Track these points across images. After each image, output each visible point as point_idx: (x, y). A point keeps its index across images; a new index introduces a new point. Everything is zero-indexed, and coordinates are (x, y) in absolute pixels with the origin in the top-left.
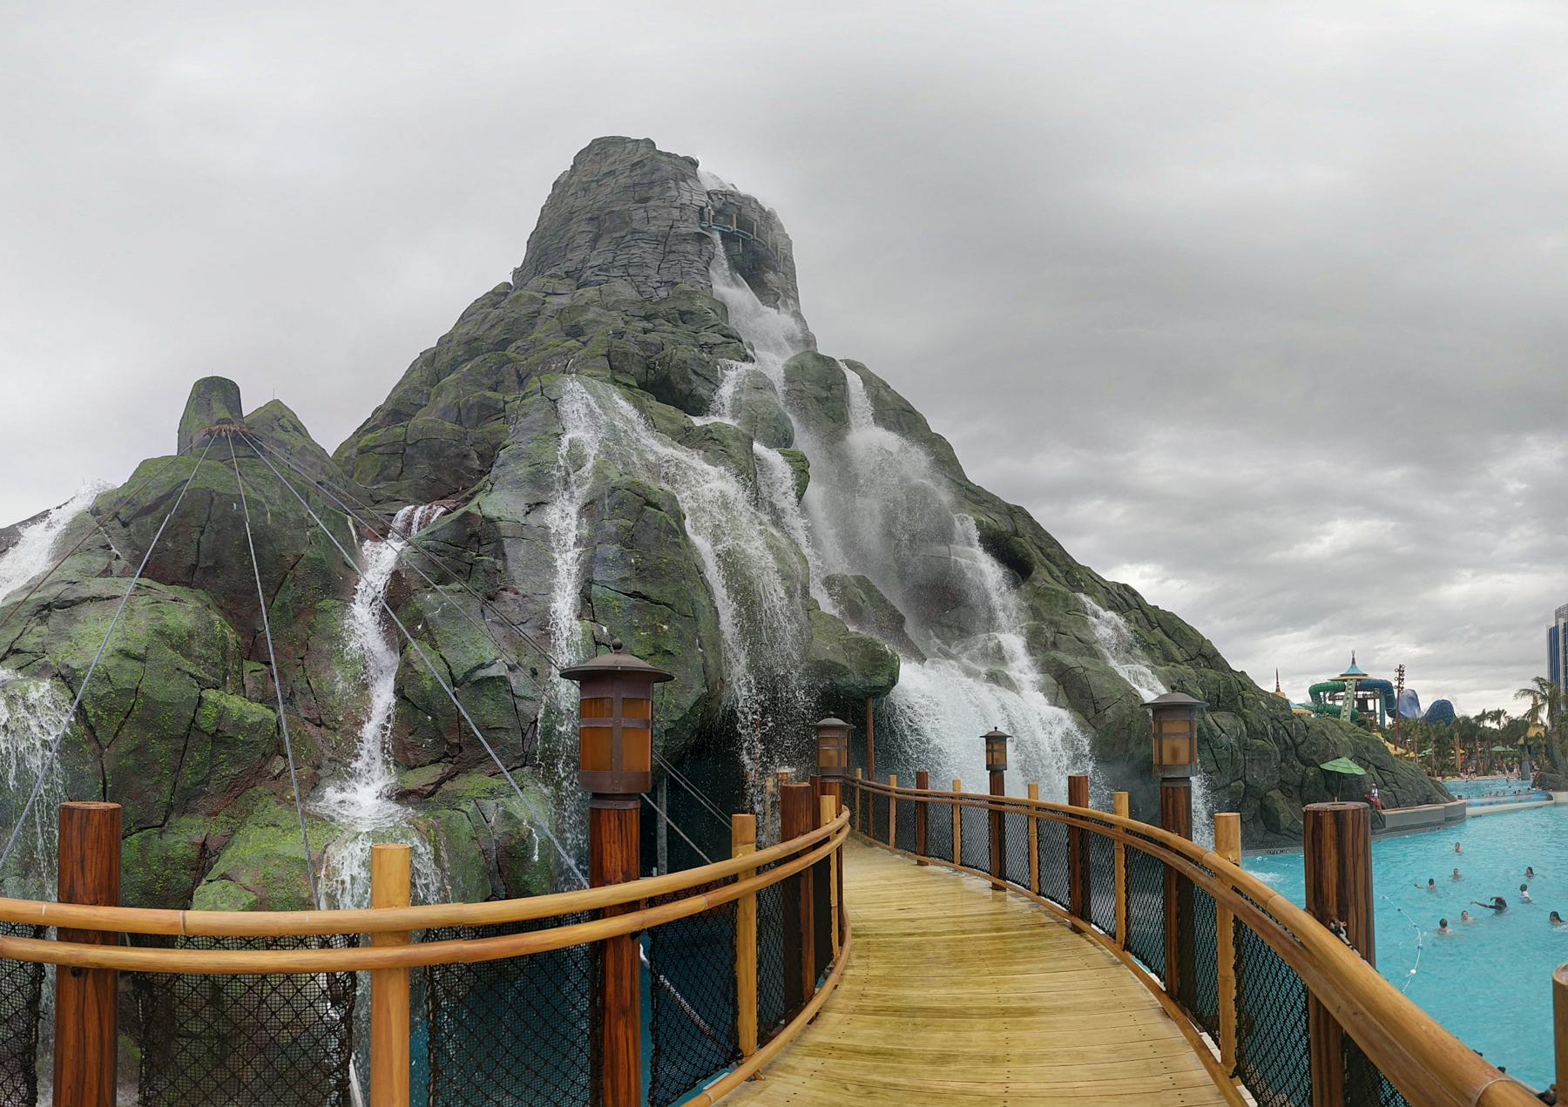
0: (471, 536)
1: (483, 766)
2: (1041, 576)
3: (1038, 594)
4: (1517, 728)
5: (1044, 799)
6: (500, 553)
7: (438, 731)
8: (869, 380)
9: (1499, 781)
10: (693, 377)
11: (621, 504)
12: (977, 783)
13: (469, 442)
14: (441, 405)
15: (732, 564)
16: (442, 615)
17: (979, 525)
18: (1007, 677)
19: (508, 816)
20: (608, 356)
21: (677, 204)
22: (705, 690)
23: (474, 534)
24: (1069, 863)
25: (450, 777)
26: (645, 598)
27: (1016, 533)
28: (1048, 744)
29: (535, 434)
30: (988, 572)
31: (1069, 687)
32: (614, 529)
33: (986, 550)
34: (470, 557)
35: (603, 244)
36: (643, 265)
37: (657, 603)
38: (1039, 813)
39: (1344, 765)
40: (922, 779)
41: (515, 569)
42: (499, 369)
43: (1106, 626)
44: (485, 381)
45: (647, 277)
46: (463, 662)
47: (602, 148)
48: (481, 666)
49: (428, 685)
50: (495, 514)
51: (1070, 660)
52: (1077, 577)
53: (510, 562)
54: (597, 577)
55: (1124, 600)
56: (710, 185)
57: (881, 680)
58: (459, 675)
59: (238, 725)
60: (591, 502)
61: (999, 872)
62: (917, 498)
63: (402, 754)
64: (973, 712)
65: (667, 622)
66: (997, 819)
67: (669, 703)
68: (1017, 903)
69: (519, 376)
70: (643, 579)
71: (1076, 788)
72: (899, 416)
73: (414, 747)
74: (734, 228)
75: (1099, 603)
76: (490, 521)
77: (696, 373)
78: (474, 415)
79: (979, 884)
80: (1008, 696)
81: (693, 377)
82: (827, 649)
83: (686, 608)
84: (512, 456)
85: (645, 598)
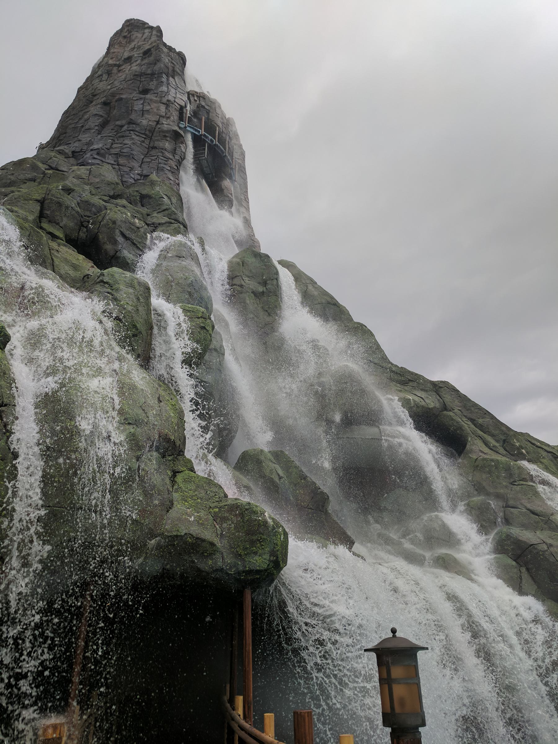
2: (477, 447)
3: (478, 466)
8: (300, 278)
10: (120, 239)
15: (57, 410)
17: (406, 403)
18: (455, 561)
21: (164, 100)
27: (445, 408)
30: (423, 449)
33: (418, 428)
35: (107, 131)
36: (130, 157)
45: (132, 169)
51: (528, 536)
56: (191, 87)
57: (259, 561)
62: (346, 380)
72: (328, 308)
74: (202, 132)
75: (547, 469)
80: (456, 584)
82: (187, 518)
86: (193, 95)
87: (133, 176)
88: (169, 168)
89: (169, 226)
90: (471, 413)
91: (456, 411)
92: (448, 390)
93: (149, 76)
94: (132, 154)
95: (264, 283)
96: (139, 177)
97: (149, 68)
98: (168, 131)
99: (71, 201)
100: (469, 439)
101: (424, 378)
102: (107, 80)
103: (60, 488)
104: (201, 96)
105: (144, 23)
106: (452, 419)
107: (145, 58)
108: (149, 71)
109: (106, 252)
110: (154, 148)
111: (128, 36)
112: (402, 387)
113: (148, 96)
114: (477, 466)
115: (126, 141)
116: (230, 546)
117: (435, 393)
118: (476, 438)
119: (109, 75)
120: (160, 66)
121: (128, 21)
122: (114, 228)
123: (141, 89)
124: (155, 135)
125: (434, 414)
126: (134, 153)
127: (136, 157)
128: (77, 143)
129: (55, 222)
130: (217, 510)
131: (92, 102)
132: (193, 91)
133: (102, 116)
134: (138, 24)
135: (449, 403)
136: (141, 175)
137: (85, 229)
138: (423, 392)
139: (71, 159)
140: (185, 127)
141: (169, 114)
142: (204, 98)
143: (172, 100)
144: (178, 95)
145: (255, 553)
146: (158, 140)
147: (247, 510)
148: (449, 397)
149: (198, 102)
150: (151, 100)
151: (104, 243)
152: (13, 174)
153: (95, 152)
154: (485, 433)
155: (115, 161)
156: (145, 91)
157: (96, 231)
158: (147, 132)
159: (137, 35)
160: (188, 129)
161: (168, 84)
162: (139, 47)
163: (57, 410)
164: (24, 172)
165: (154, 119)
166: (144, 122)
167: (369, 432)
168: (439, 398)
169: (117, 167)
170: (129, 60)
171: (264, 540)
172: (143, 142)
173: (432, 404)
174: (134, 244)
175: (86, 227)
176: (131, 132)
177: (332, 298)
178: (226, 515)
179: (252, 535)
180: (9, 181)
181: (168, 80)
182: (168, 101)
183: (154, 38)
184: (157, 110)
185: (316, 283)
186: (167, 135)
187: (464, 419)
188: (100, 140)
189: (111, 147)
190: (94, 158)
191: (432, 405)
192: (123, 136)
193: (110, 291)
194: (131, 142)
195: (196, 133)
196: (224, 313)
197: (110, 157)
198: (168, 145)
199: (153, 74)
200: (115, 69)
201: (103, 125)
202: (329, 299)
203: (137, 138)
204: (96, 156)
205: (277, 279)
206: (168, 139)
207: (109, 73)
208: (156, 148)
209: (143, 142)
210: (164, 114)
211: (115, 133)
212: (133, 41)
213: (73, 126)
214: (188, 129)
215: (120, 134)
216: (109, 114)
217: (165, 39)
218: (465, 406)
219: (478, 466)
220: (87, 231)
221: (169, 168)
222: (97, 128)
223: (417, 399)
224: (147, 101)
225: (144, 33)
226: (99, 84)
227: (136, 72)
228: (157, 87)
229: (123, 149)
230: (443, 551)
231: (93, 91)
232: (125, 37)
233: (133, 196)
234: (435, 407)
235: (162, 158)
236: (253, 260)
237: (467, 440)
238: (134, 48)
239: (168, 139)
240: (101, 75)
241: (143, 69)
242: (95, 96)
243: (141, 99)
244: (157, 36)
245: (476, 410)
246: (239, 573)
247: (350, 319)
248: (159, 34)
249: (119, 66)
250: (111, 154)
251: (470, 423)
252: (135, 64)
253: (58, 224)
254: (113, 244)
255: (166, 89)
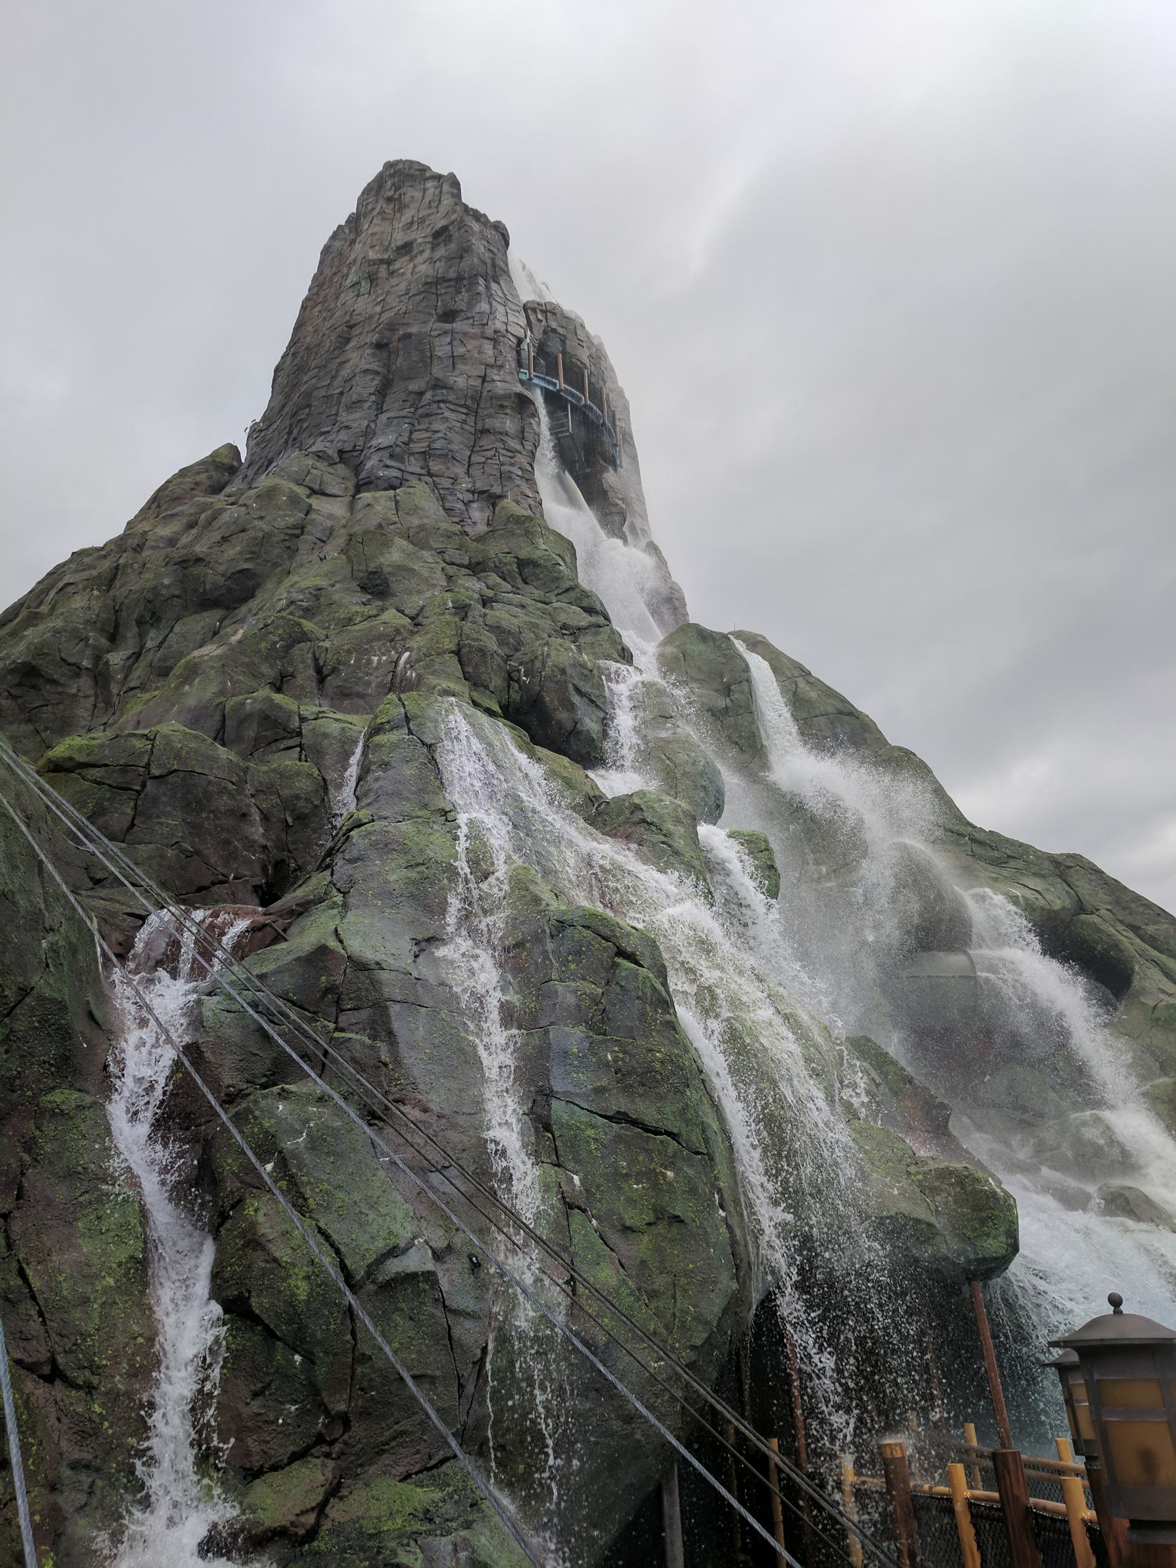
0: (327, 991)
1: (386, 1459)
6: (381, 1028)
7: (313, 1389)
10: (576, 699)
11: (579, 953)
13: (249, 789)
14: (191, 702)
16: (314, 1144)
20: (457, 653)
21: (489, 332)
22: (735, 1286)
23: (330, 989)
25: (334, 1491)
26: (635, 1123)
27: (1081, 907)
29: (407, 807)
32: (571, 1000)
35: (393, 407)
36: (448, 457)
37: (657, 1132)
41: (416, 1063)
42: (288, 648)
44: (265, 669)
46: (362, 1246)
48: (393, 1252)
49: (302, 1289)
50: (369, 955)
53: (403, 1049)
54: (558, 1086)
56: (526, 295)
57: (993, 1246)
58: (358, 1268)
60: (519, 945)
65: (670, 1165)
67: (685, 1312)
69: (319, 670)
70: (627, 1089)
73: (261, 1423)
76: (362, 967)
77: (578, 691)
78: (250, 732)
81: (576, 699)
83: (696, 1139)
84: (374, 845)
85: (635, 1123)
86: (534, 310)
87: (460, 496)
88: (520, 473)
89: (597, 634)
90: (1131, 914)
91: (1103, 912)
92: (1083, 871)
93: (453, 283)
94: (451, 451)
95: (727, 691)
96: (470, 497)
97: (450, 267)
98: (506, 397)
100: (1137, 968)
101: (1036, 851)
102: (369, 293)
104: (550, 310)
105: (424, 169)
106: (1099, 930)
107: (438, 245)
108: (452, 274)
109: (560, 725)
110: (485, 431)
111: (396, 196)
112: (997, 869)
113: (458, 325)
114: (1158, 1020)
115: (437, 426)
116: (953, 1226)
117: (1059, 880)
118: (1148, 964)
119: (371, 281)
120: (471, 261)
121: (389, 165)
122: (565, 682)
123: (440, 311)
124: (482, 405)
125: (1063, 921)
126: (454, 447)
127: (457, 456)
128: (343, 432)
129: (482, 685)
130: (920, 1177)
131: (348, 340)
132: (533, 302)
133: (378, 373)
134: (412, 172)
135: (1087, 898)
136: (473, 492)
137: (516, 686)
138: (1038, 880)
139: (339, 466)
140: (530, 379)
141: (500, 358)
142: (554, 314)
143: (502, 328)
144: (511, 318)
145: (988, 1235)
146: (490, 416)
147: (966, 1177)
148: (1087, 886)
149: (544, 323)
150: (465, 334)
151: (555, 709)
152: (261, 518)
153: (386, 453)
154: (1161, 952)
155: (422, 468)
156: (449, 316)
157: (538, 688)
158: (469, 402)
159: (411, 193)
160: (536, 381)
161: (490, 296)
162: (422, 221)
164: (281, 513)
165: (476, 373)
166: (461, 382)
168: (1067, 888)
169: (428, 479)
170: (406, 248)
171: (997, 1217)
172: (464, 422)
173: (1058, 901)
174: (592, 702)
175: (518, 681)
176: (442, 405)
177: (844, 701)
178: (937, 1184)
179: (981, 1211)
180: (261, 534)
181: (488, 288)
182: (496, 332)
183: (447, 201)
184: (479, 352)
185: (810, 674)
186: (506, 404)
187: (1121, 927)
188: (388, 425)
189: (411, 440)
190: (387, 466)
191: (1057, 905)
192: (427, 415)
193: (665, 839)
194: (446, 425)
195: (551, 388)
197: (412, 458)
198: (509, 424)
199: (459, 279)
200: (383, 271)
201: (382, 392)
202: (840, 706)
203: (453, 416)
204: (389, 462)
205: (748, 681)
206: (508, 411)
207: (372, 279)
208: (488, 431)
209: (464, 422)
210: (492, 361)
211: (412, 410)
212: (407, 206)
213: (323, 392)
214: (536, 381)
215: (420, 411)
216: (387, 366)
217: (466, 199)
218: (1117, 902)
220: (520, 688)
221: (520, 473)
222: (373, 398)
223: (1029, 894)
224: (458, 336)
225: (425, 190)
226: (355, 302)
227: (427, 276)
228: (471, 305)
229: (433, 442)
230: (1117, 1182)
231: (348, 317)
232: (389, 200)
233: (506, 564)
234: (1064, 908)
235: (504, 452)
236: (702, 647)
237: (1132, 969)
238: (412, 223)
239: (508, 411)
240: (358, 283)
241: (441, 271)
242: (351, 327)
243: (446, 332)
244: (453, 195)
245: (1141, 909)
246: (969, 1262)
247: (881, 740)
248: (455, 191)
249: (389, 262)
250: (413, 454)
251: (1131, 934)
252: (420, 259)
253: (487, 687)
254: (568, 710)
255: (488, 306)
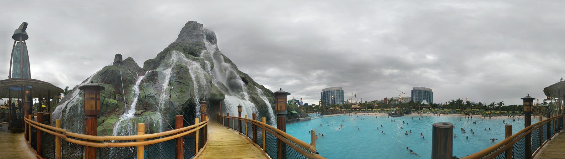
2: (250, 84)
4: (317, 106)
5: (248, 118)
9: (315, 114)
12: (237, 115)
15: (197, 78)
19: (151, 118)
24: (252, 130)
28: (248, 108)
30: (242, 83)
31: (254, 100)
34: (153, 78)
38: (247, 121)
39: (294, 112)
40: (228, 114)
43: (259, 91)
46: (147, 93)
47: (189, 23)
51: (254, 96)
52: (255, 84)
55: (262, 87)
57: (222, 98)
59: (110, 104)
61: (241, 131)
63: (137, 108)
64: (238, 104)
66: (240, 121)
68: (243, 137)
71: (254, 115)
79: (237, 133)
82: (214, 91)
99: (188, 48)
103: (200, 87)
163: (197, 78)
167: (234, 80)
196: (214, 61)
219: (249, 86)
